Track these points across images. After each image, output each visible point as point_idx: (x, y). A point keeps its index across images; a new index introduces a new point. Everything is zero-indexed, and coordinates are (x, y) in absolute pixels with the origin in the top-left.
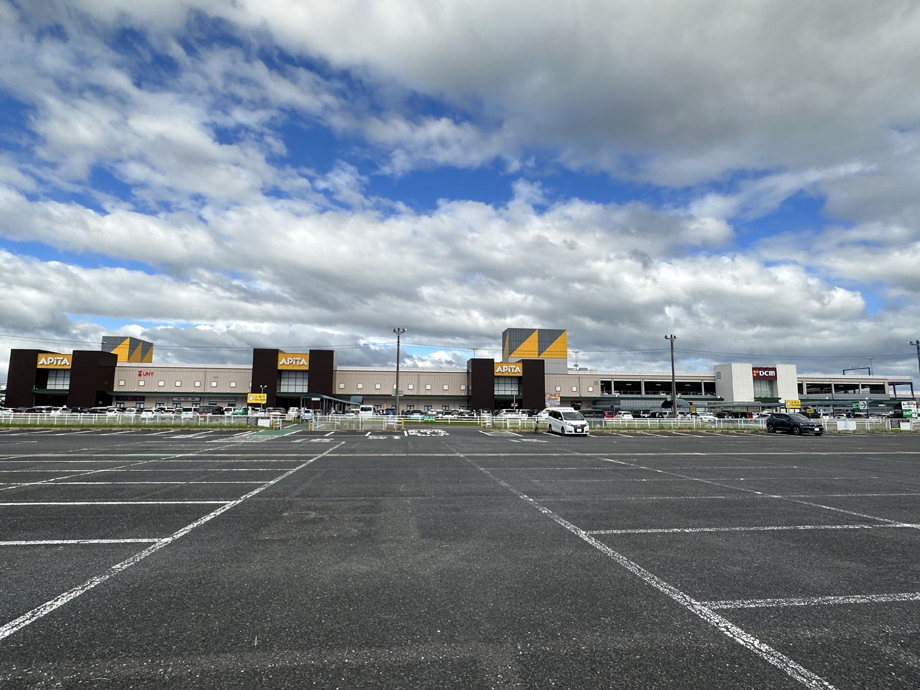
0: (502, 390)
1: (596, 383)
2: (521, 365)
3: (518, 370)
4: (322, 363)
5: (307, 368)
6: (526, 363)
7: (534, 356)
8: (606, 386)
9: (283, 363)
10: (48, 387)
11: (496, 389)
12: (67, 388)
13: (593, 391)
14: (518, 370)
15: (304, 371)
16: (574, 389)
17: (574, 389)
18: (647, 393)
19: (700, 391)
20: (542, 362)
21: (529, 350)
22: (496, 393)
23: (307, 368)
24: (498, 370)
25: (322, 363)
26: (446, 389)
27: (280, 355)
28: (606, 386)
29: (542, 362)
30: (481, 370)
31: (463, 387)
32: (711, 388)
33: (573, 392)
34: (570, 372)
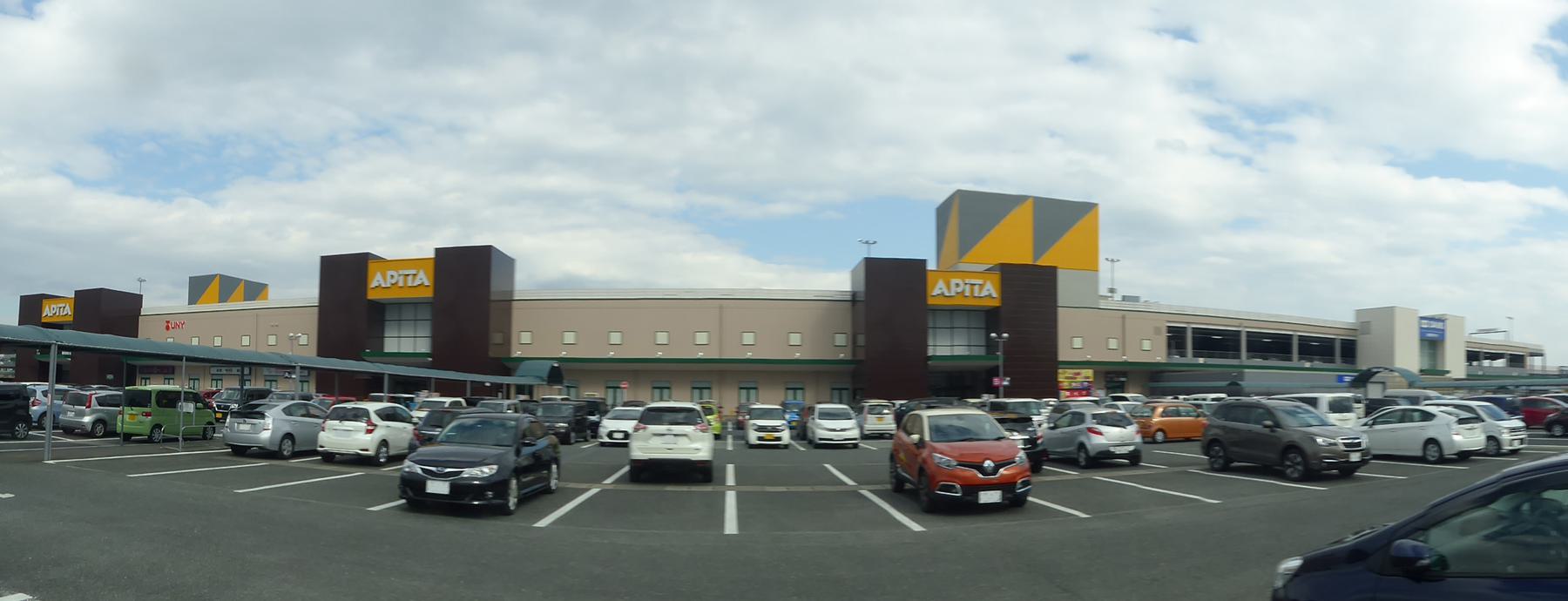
0: (946, 346)
1: (1157, 331)
2: (997, 277)
3: (989, 292)
4: (468, 276)
5: (429, 293)
6: (1009, 274)
7: (1021, 254)
8: (1176, 338)
9: (379, 284)
10: (391, 346)
11: (930, 342)
12: (727, 532)
13: (1152, 350)
14: (989, 292)
15: (415, 304)
16: (1113, 344)
17: (1113, 344)
18: (1196, 355)
19: (1237, 349)
20: (1050, 273)
21: (1012, 243)
22: (930, 353)
23: (429, 293)
24: (938, 290)
25: (468, 276)
26: (796, 345)
27: (372, 266)
28: (1176, 338)
29: (1050, 273)
30: (891, 288)
31: (841, 340)
32: (1349, 349)
33: (1112, 351)
34: (1103, 304)
